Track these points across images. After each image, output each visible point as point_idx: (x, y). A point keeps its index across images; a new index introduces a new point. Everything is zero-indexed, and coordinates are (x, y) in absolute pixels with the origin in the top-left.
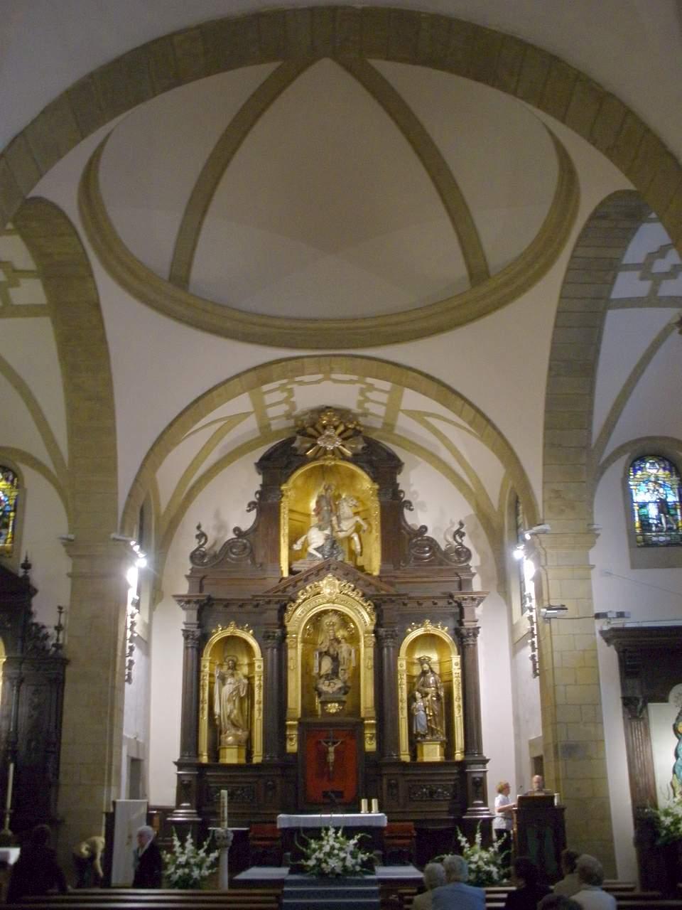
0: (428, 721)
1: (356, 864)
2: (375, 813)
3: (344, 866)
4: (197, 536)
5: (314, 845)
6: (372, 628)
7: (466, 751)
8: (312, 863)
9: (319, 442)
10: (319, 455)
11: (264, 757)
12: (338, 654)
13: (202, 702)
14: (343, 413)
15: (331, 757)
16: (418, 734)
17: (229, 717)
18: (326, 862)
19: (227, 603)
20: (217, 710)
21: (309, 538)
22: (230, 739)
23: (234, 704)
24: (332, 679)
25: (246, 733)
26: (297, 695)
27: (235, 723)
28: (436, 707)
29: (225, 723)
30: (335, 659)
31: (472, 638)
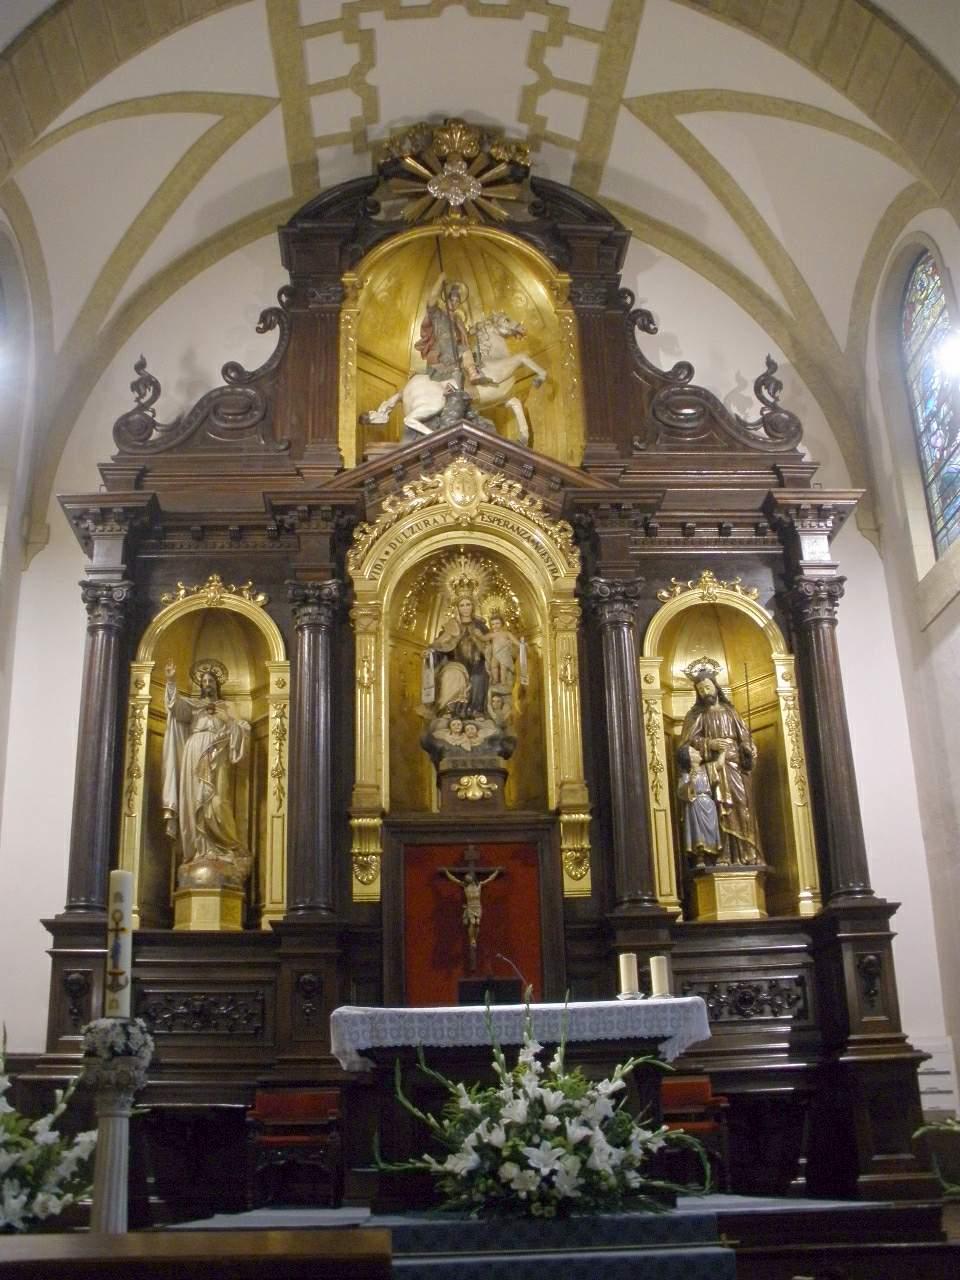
0: (721, 819)
1: (627, 1164)
2: (660, 996)
3: (586, 1171)
4: (135, 387)
5: (467, 1101)
6: (571, 584)
7: (827, 889)
8: (462, 1163)
9: (431, 190)
10: (427, 217)
11: (292, 909)
12: (483, 658)
13: (131, 775)
14: (487, 135)
15: (474, 912)
16: (699, 854)
17: (199, 813)
18: (523, 1163)
19: (203, 529)
20: (169, 798)
21: (406, 400)
22: (202, 873)
23: (214, 781)
24: (471, 717)
25: (247, 861)
26: (378, 752)
27: (216, 830)
28: (741, 787)
29: (190, 831)
30: (476, 667)
31: (826, 605)
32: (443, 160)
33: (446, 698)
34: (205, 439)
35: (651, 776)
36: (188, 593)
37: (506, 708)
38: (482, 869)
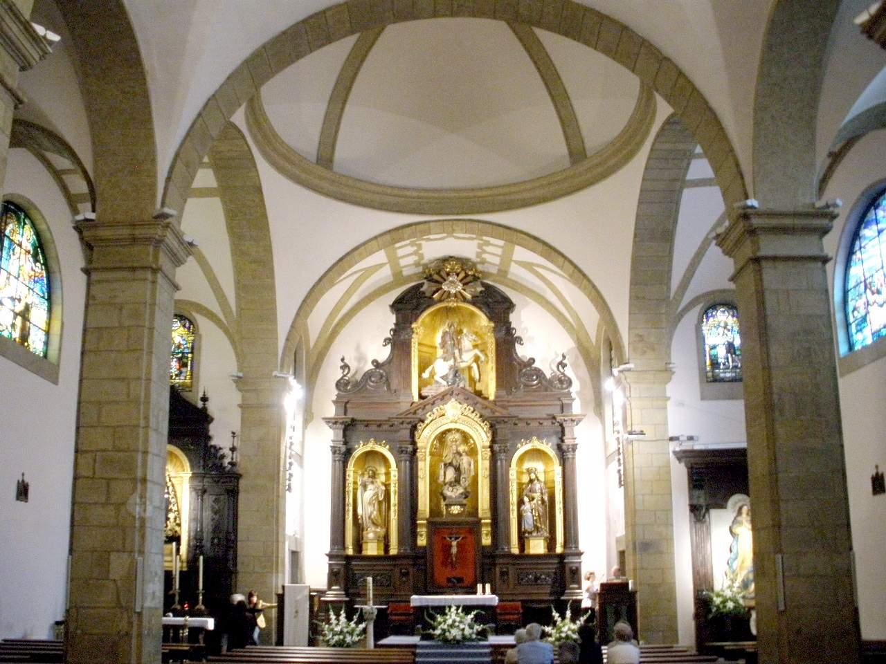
3: (463, 635)
4: (341, 367)
5: (439, 618)
7: (565, 545)
8: (438, 632)
15: (454, 550)
17: (370, 517)
20: (360, 511)
25: (384, 530)
29: (366, 522)
30: (458, 470)
32: (448, 274)
33: (447, 480)
34: (367, 389)
35: (511, 507)
36: (364, 445)
37: (465, 482)
38: (457, 536)
